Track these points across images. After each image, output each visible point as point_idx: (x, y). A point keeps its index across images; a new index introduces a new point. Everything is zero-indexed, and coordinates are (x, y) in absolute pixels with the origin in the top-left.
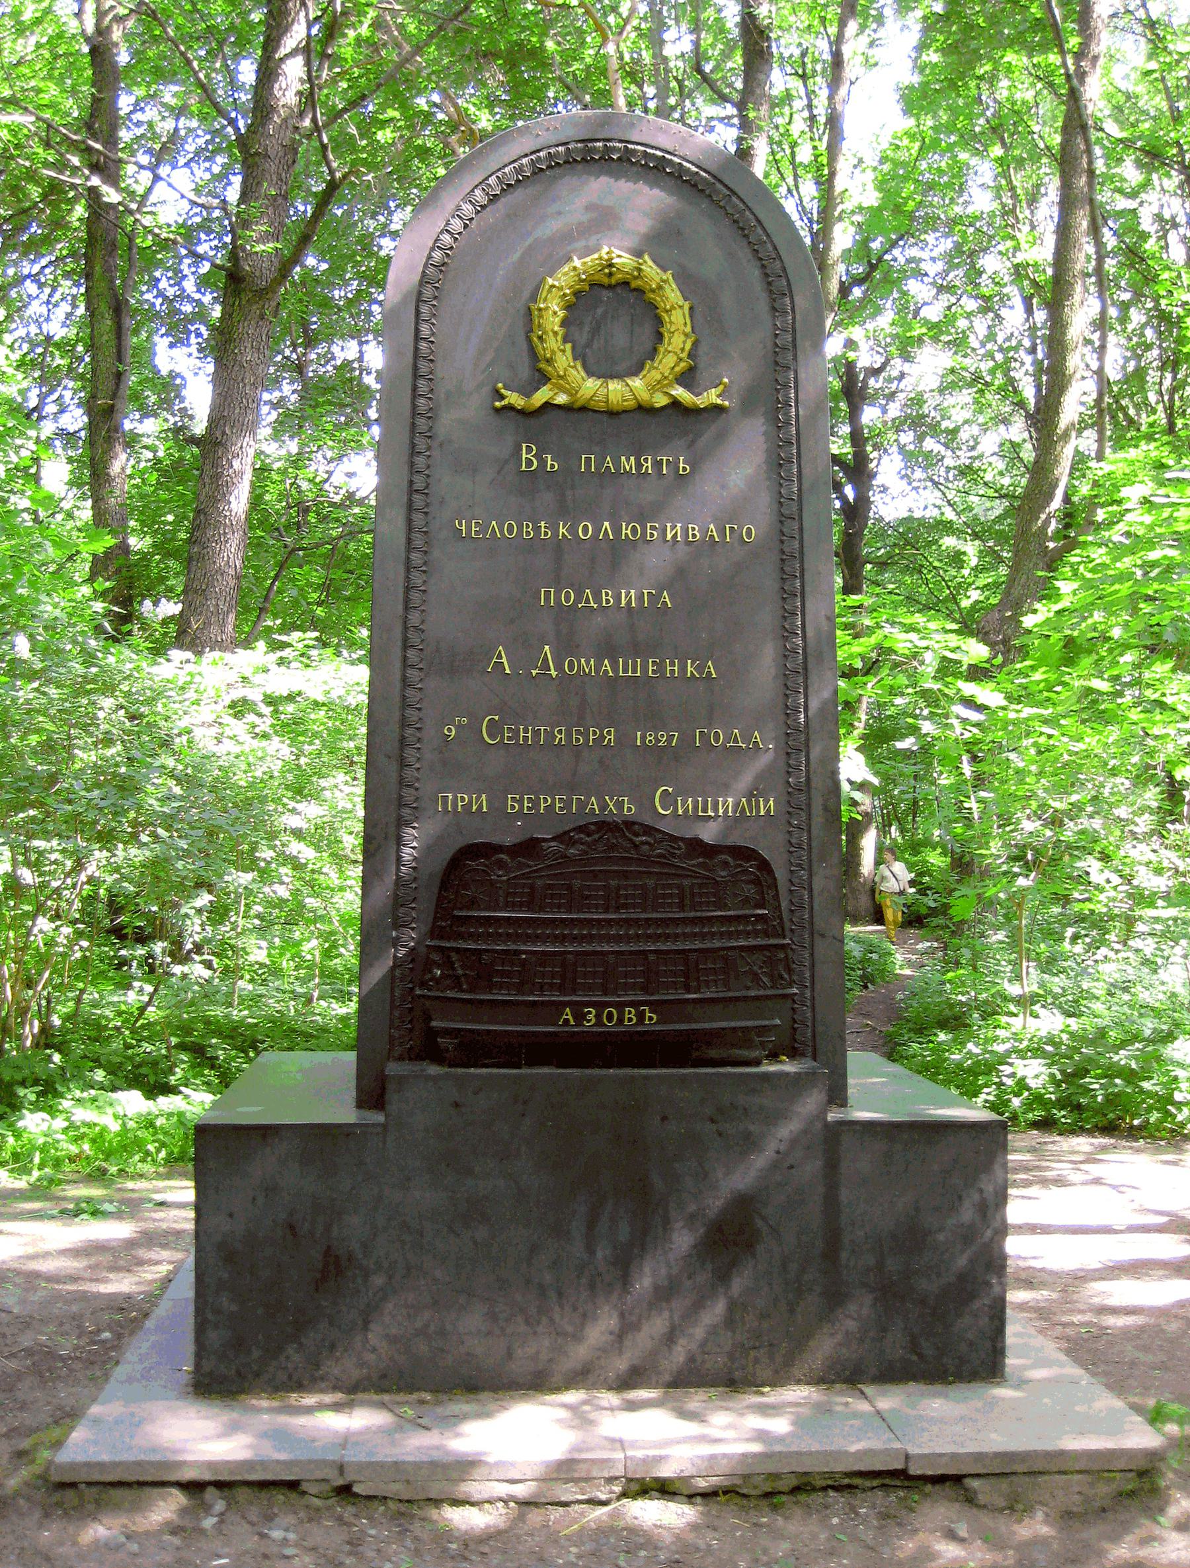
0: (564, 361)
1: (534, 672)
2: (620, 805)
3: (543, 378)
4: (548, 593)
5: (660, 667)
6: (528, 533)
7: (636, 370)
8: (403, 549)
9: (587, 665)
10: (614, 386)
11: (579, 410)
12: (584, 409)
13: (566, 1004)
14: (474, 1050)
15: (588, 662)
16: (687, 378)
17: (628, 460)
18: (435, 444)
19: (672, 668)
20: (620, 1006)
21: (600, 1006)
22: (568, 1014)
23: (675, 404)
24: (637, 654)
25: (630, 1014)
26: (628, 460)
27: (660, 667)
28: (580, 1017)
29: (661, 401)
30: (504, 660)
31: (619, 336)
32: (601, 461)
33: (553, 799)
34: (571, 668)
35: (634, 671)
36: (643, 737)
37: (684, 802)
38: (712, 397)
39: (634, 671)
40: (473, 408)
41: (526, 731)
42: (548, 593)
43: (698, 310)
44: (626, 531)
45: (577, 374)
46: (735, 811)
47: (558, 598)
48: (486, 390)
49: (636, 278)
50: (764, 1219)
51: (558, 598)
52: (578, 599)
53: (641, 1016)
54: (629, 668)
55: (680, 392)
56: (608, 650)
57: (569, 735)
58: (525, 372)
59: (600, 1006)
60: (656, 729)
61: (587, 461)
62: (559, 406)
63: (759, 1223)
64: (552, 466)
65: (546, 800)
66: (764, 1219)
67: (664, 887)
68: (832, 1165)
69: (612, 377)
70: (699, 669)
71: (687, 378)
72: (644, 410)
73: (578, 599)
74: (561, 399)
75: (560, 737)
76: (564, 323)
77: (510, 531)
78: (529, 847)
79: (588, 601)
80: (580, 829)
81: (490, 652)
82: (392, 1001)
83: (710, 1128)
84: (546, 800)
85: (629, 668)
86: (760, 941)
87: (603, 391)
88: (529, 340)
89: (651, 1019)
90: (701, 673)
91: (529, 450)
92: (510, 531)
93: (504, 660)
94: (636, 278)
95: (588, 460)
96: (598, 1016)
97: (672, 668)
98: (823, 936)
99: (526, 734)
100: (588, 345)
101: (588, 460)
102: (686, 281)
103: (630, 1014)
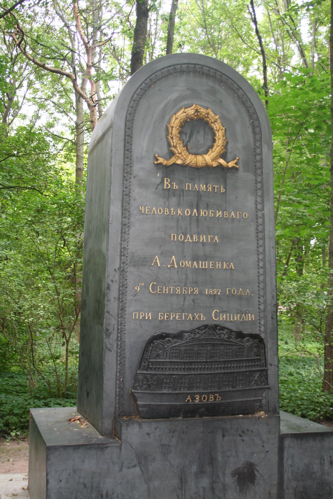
0: (180, 149)
1: (169, 266)
2: (199, 317)
3: (172, 154)
4: (174, 236)
5: (214, 264)
6: (167, 213)
7: (206, 152)
8: (254, 210)
9: (188, 263)
10: (199, 158)
11: (183, 166)
12: (187, 166)
13: (188, 394)
14: (154, 414)
15: (188, 263)
16: (223, 156)
17: (203, 186)
18: (132, 177)
19: (218, 265)
20: (208, 394)
21: (201, 394)
22: (189, 398)
23: (220, 166)
24: (206, 260)
25: (212, 397)
26: (203, 186)
27: (214, 264)
28: (193, 399)
29: (215, 164)
30: (158, 261)
31: (200, 138)
32: (193, 187)
33: (176, 315)
34: (182, 265)
35: (205, 266)
36: (208, 291)
37: (223, 316)
38: (231, 164)
39: (205, 266)
40: (148, 163)
41: (219, 264)
42: (174, 236)
43: (227, 133)
44: (202, 213)
45: (185, 153)
46: (240, 319)
47: (177, 238)
48: (152, 158)
49: (206, 117)
50: (258, 471)
51: (177, 238)
52: (185, 238)
53: (215, 398)
54: (204, 265)
55: (222, 161)
56: (196, 258)
57: (181, 290)
58: (165, 151)
59: (201, 394)
60: (213, 288)
61: (188, 186)
62: (178, 165)
63: (256, 473)
64: (176, 187)
65: (173, 315)
66: (258, 471)
67: (227, 349)
68: (281, 450)
69: (197, 154)
70: (228, 266)
71: (223, 156)
72: (207, 168)
73: (185, 238)
74: (179, 162)
75: (178, 291)
76: (180, 133)
77: (160, 211)
78: (179, 336)
79: (188, 239)
80: (199, 328)
81: (152, 257)
82: (116, 394)
83: (240, 438)
84: (173, 315)
85: (204, 265)
86: (259, 368)
87: (195, 160)
88: (167, 139)
89: (219, 398)
90: (229, 267)
91: (167, 181)
92: (160, 211)
93: (158, 261)
94: (206, 117)
95: (189, 186)
96: (200, 398)
97: (218, 265)
98: (271, 365)
99: (166, 290)
100: (189, 141)
101: (189, 186)
102: (224, 120)
103: (212, 397)
